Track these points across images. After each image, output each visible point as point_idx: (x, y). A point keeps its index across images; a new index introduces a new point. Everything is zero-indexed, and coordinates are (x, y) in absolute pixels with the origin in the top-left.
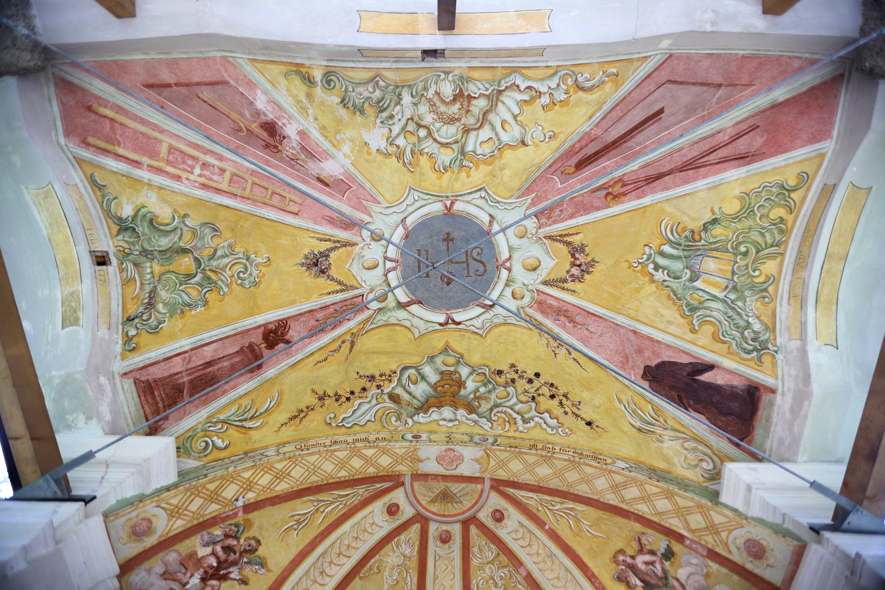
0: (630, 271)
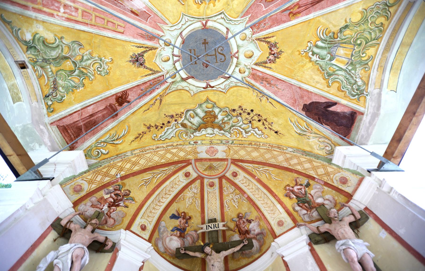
0: (300, 56)
